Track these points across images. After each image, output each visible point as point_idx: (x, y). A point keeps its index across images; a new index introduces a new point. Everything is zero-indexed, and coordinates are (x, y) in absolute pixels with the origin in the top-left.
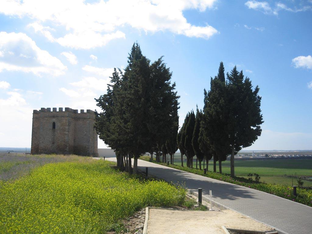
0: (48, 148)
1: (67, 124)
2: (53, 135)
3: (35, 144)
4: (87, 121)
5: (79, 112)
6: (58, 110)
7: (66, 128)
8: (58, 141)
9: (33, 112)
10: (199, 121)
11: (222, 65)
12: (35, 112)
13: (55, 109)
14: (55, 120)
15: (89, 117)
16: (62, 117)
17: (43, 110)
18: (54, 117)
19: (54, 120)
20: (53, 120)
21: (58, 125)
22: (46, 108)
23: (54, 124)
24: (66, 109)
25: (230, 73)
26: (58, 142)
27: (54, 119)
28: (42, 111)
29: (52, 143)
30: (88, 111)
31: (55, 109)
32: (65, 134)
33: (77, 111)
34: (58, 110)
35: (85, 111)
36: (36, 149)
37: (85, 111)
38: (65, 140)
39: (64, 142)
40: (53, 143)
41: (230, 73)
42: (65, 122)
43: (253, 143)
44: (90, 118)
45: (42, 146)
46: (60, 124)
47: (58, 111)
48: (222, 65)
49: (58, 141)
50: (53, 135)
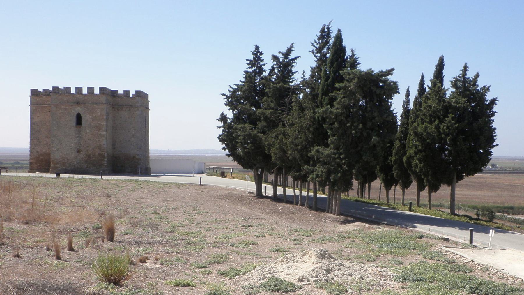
0: (68, 160)
1: (105, 117)
2: (77, 137)
3: (37, 152)
4: (136, 111)
5: (73, 91)
6: (85, 91)
7: (102, 124)
8: (88, 149)
9: (29, 93)
10: (405, 134)
11: (441, 60)
12: (34, 93)
13: (79, 90)
14: (80, 109)
15: (139, 105)
16: (93, 103)
17: (57, 91)
18: (78, 103)
19: (79, 109)
20: (76, 109)
21: (86, 118)
22: (62, 87)
23: (79, 119)
24: (102, 89)
25: (430, 86)
26: (88, 150)
27: (79, 108)
28: (55, 93)
29: (76, 150)
30: (102, 89)
31: (79, 90)
32: (101, 135)
33: (68, 89)
34: (85, 91)
35: (97, 91)
36: (40, 162)
37: (97, 91)
38: (100, 145)
39: (100, 149)
40: (79, 151)
41: (430, 86)
42: (99, 114)
43: (496, 136)
44: (141, 106)
45: (56, 156)
46: (91, 117)
47: (98, 93)
48: (441, 60)
49: (88, 149)
50: (77, 137)
